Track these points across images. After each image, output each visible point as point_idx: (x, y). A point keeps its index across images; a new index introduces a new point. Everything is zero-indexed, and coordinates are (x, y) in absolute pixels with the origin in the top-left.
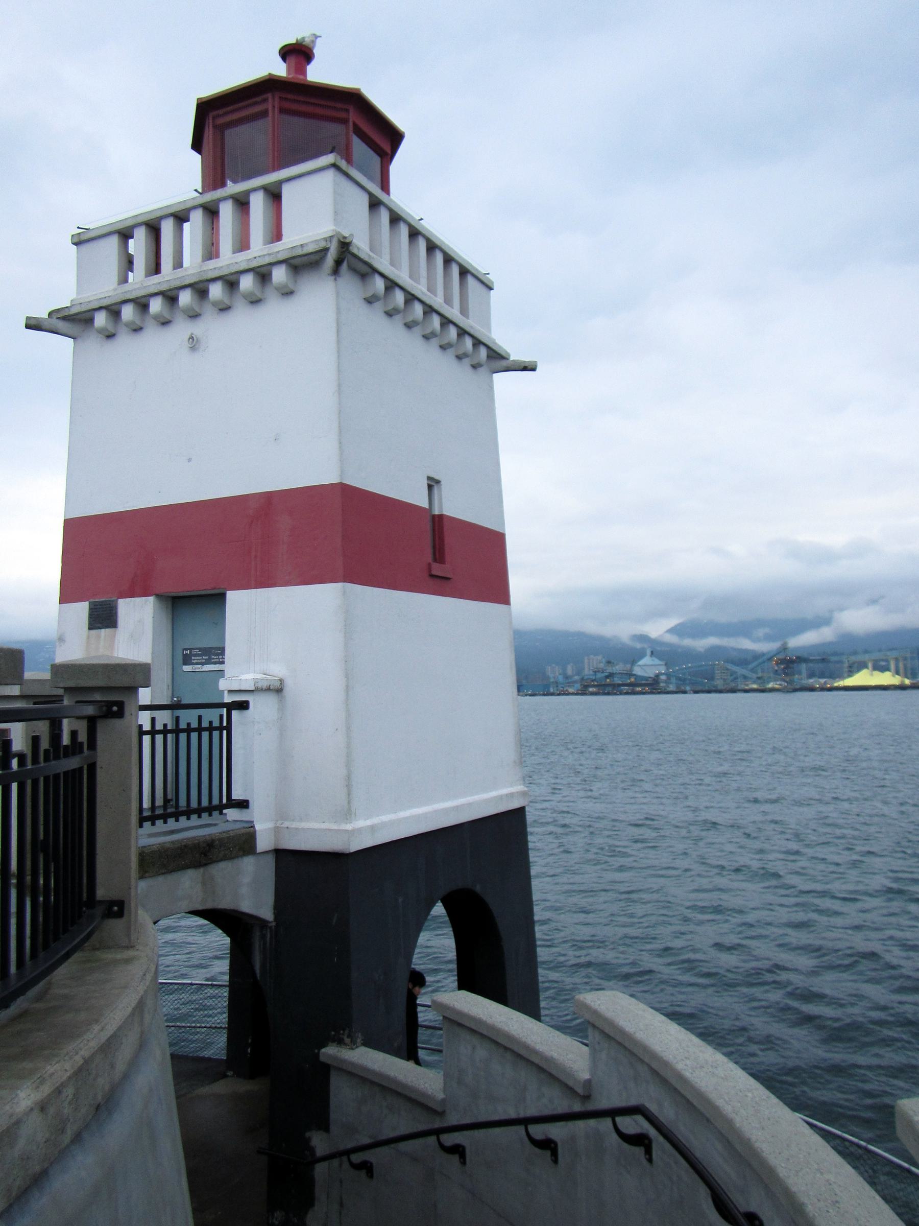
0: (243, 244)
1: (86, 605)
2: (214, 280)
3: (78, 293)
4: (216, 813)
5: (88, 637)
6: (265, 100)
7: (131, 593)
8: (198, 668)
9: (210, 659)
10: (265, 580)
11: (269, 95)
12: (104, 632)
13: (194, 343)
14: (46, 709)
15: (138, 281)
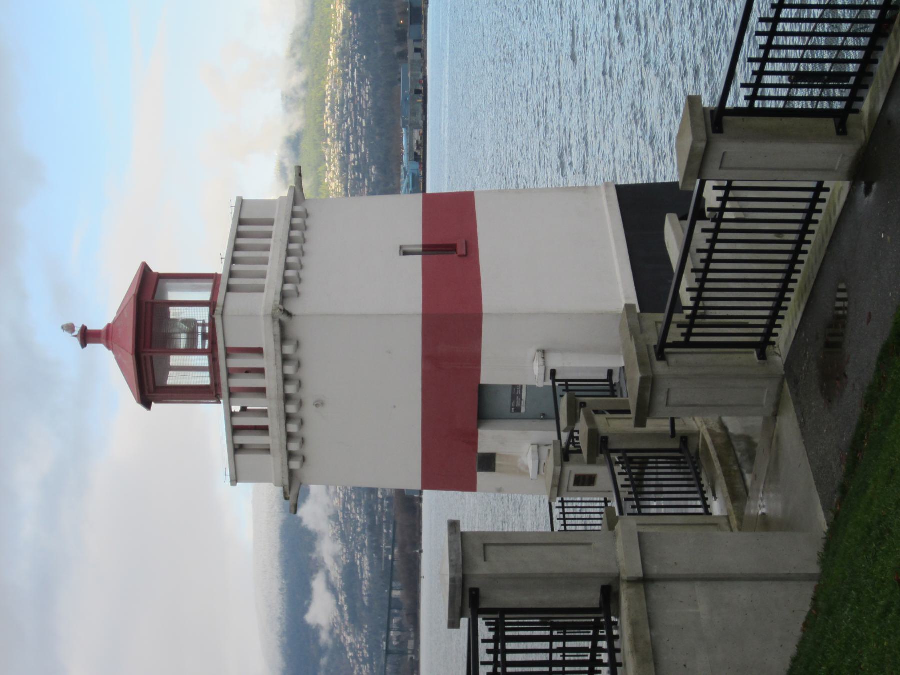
3: (270, 482)
4: (615, 388)
7: (475, 444)
8: (523, 403)
10: (476, 360)
12: (497, 462)
13: (319, 404)
14: (671, 284)
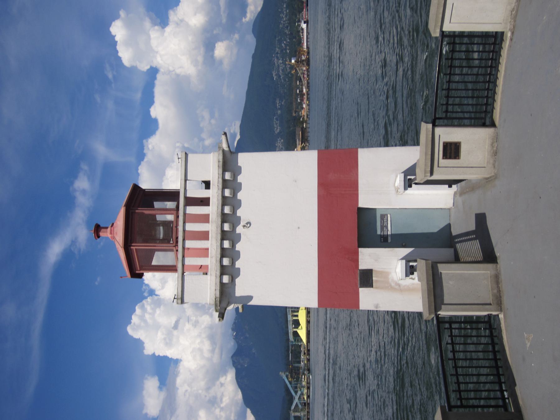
2: (223, 210)
5: (376, 288)
7: (356, 261)
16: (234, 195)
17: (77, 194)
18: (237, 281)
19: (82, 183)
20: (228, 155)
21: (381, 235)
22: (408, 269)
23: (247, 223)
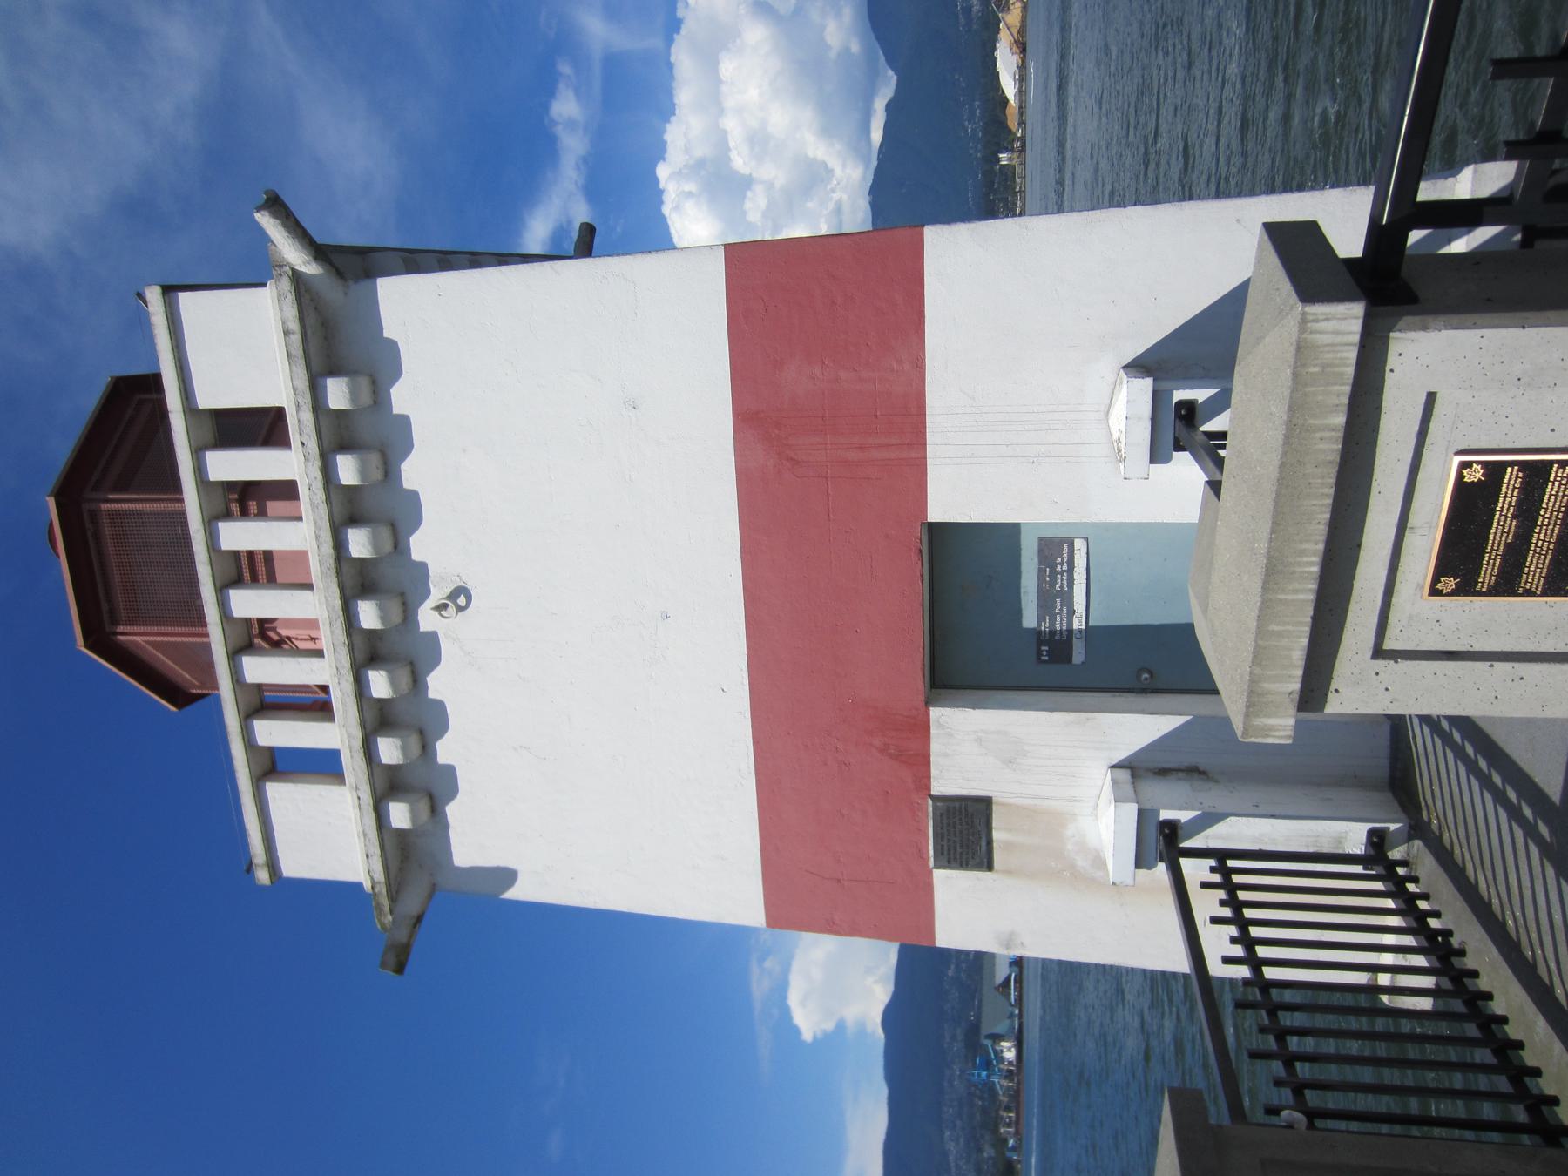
0: (316, 705)
1: (940, 876)
5: (1008, 872)
6: (94, 515)
7: (920, 762)
9: (1061, 594)
10: (905, 421)
11: (86, 507)
15: (336, 734)
16: (386, 474)
17: (559, 130)
18: (452, 810)
19: (566, 107)
20: (331, 291)
21: (1037, 633)
22: (1152, 834)
23: (454, 595)
